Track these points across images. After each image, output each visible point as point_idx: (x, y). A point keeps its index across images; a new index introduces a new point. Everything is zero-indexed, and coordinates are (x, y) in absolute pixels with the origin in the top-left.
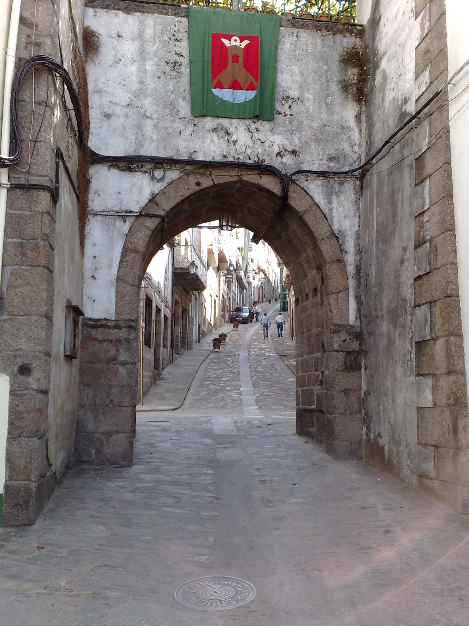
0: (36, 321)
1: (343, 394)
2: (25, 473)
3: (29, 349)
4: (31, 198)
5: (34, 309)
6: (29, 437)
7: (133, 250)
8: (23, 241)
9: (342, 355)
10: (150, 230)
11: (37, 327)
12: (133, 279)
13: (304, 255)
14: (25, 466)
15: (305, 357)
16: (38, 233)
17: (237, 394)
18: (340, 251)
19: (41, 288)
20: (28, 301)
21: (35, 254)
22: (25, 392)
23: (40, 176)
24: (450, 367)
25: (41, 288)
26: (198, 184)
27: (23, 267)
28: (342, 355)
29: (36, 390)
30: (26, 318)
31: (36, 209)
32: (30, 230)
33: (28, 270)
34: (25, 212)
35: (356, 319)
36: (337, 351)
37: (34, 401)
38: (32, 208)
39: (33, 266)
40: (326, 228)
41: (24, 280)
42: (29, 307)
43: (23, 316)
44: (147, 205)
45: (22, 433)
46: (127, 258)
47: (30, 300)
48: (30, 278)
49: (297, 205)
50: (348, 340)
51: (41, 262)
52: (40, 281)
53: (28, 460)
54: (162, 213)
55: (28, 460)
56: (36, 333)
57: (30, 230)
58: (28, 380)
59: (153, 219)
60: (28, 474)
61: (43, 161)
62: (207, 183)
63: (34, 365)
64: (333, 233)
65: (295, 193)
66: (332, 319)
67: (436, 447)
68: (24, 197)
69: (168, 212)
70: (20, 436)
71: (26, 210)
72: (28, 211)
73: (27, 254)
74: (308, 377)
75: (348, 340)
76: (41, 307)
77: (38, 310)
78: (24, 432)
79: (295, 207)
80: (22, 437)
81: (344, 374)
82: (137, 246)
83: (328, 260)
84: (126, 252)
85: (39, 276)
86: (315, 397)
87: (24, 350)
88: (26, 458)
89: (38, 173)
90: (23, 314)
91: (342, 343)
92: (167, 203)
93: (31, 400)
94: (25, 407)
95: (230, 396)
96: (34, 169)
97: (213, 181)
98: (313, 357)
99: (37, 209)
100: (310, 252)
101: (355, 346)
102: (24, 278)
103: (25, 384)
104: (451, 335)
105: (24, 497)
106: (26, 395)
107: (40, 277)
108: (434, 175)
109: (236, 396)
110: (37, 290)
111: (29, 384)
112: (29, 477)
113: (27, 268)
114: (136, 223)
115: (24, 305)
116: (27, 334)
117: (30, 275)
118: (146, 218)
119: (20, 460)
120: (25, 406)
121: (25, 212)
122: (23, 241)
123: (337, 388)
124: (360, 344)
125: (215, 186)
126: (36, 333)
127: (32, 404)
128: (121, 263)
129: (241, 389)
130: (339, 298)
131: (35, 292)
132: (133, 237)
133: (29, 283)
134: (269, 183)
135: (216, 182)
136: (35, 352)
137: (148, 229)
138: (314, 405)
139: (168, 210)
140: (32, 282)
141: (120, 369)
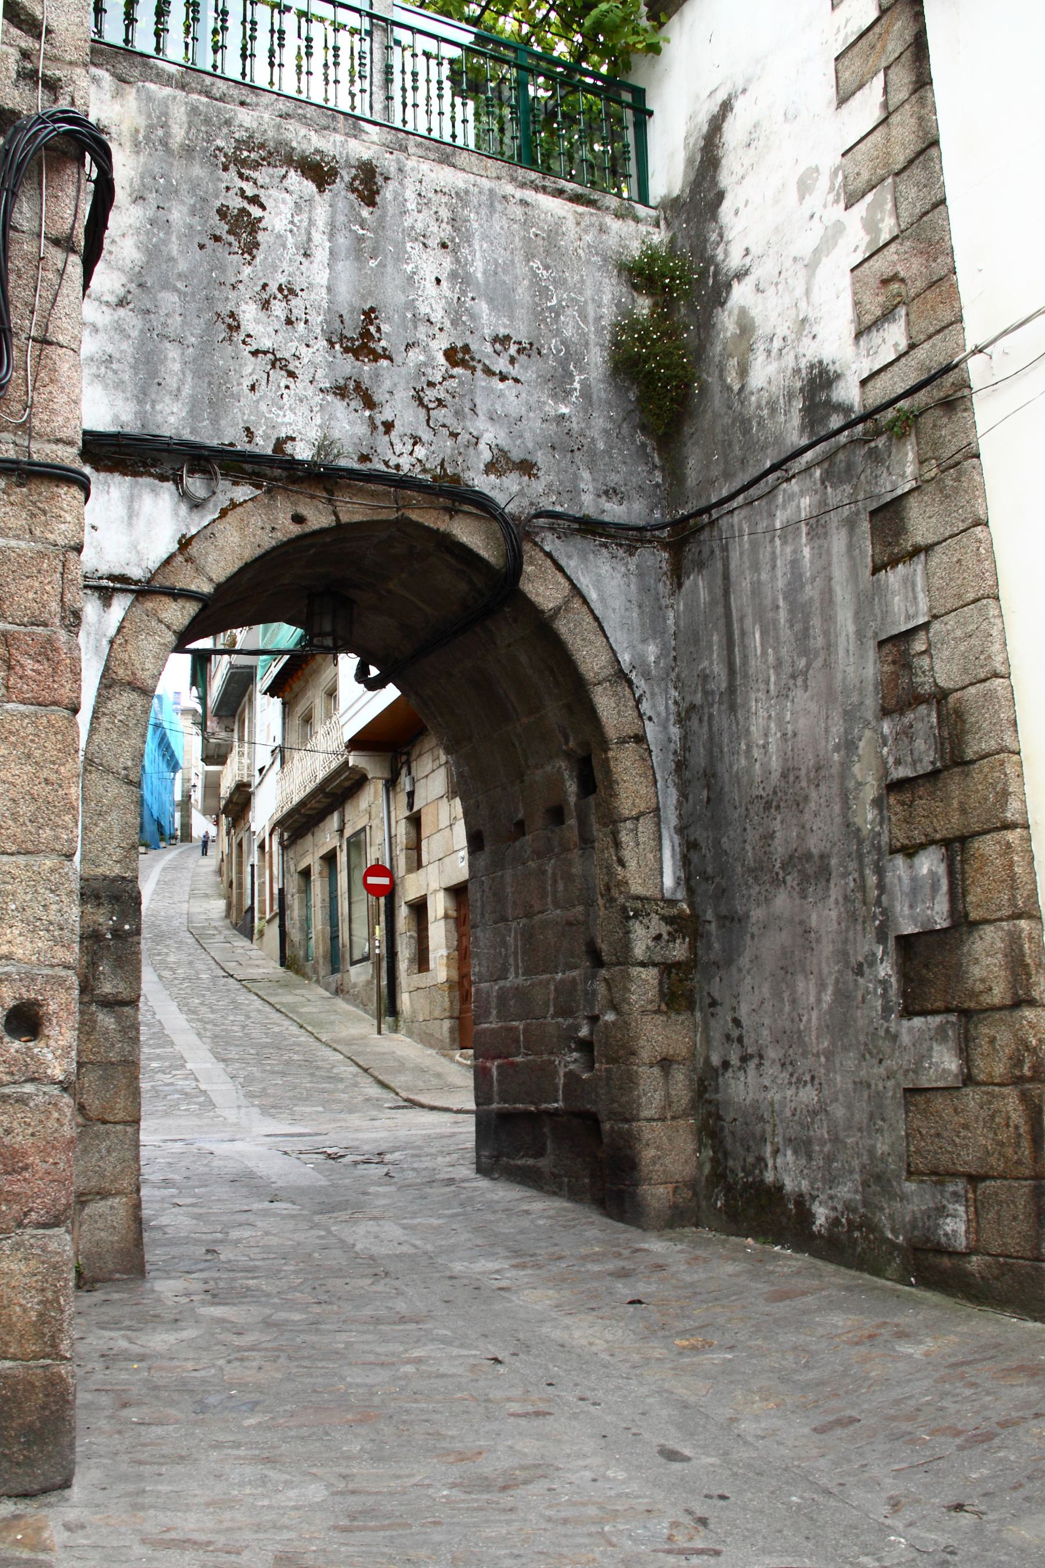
0: (52, 871)
1: (656, 1071)
2: (44, 1335)
3: (34, 958)
4: (34, 503)
5: (47, 833)
6: (45, 1226)
7: (129, 683)
8: (9, 627)
9: (654, 972)
10: (174, 632)
11: (58, 889)
12: (129, 763)
13: (525, 720)
14: (40, 1315)
15: (513, 980)
16: (55, 606)
17: (186, 1079)
18: (636, 714)
19: (62, 769)
20: (25, 809)
21: (45, 667)
22: (29, 1088)
23: (58, 441)
24: (1021, 992)
25: (62, 769)
26: (298, 519)
27: (9, 706)
28: (654, 972)
29: (61, 1082)
30: (21, 860)
31: (49, 536)
32: (31, 595)
33: (24, 716)
34: (13, 543)
35: (679, 884)
36: (643, 964)
37: (56, 1115)
38: (37, 533)
39: (40, 704)
40: (604, 658)
41: (14, 745)
42: (30, 827)
43: (12, 854)
44: (168, 561)
45: (26, 1214)
46: (112, 706)
47: (33, 808)
48: (32, 741)
49: (538, 595)
50: (665, 937)
51: (62, 691)
52: (59, 750)
53: (49, 1295)
54: (207, 588)
55: (49, 1295)
56: (54, 907)
57: (31, 595)
58: (36, 1050)
59: (181, 602)
60: (53, 1337)
61: (66, 399)
62: (319, 518)
63: (53, 1007)
64: (621, 670)
65: (531, 564)
66: (626, 883)
67: (974, 1179)
68: (12, 498)
69: (219, 587)
70: (20, 1225)
71: (17, 537)
72: (24, 539)
73: (22, 666)
74: (525, 1031)
75: (665, 937)
76: (66, 828)
77: (57, 838)
78: (31, 1210)
79: (533, 597)
80: (25, 1227)
81: (660, 1019)
82: (139, 673)
83: (612, 734)
84: (110, 687)
85: (56, 734)
86: (561, 1081)
87: (19, 960)
88: (43, 1290)
89: (53, 431)
90: (14, 848)
91: (651, 944)
92: (217, 561)
93: (48, 1114)
94: (33, 1135)
95: (171, 1084)
96: (41, 420)
97: (337, 517)
98: (548, 982)
99: (51, 537)
100: (553, 713)
101: (679, 951)
102: (13, 739)
103: (27, 1065)
104: (1019, 916)
105: (43, 1408)
106: (30, 1096)
107: (59, 737)
108: (938, 549)
109: (188, 1085)
110: (53, 777)
111: (40, 1063)
112: (54, 1346)
113: (22, 708)
114: (138, 610)
115: (15, 820)
116: (29, 912)
117: (30, 730)
118: (166, 600)
119: (24, 1298)
120: (30, 1131)
121: (13, 543)
122: (9, 627)
123: (645, 1055)
124: (693, 948)
125: (339, 526)
126: (54, 907)
127: (52, 1124)
128: (97, 718)
129: (189, 1066)
130: (640, 829)
131: (47, 781)
132: (129, 647)
133: (29, 756)
134: (468, 533)
135: (344, 518)
136: (52, 966)
137: (168, 627)
138: (556, 1101)
139: (222, 579)
140: (37, 753)
141: (101, 1016)
